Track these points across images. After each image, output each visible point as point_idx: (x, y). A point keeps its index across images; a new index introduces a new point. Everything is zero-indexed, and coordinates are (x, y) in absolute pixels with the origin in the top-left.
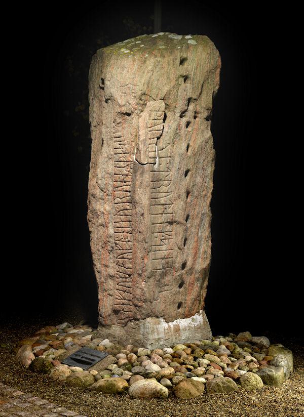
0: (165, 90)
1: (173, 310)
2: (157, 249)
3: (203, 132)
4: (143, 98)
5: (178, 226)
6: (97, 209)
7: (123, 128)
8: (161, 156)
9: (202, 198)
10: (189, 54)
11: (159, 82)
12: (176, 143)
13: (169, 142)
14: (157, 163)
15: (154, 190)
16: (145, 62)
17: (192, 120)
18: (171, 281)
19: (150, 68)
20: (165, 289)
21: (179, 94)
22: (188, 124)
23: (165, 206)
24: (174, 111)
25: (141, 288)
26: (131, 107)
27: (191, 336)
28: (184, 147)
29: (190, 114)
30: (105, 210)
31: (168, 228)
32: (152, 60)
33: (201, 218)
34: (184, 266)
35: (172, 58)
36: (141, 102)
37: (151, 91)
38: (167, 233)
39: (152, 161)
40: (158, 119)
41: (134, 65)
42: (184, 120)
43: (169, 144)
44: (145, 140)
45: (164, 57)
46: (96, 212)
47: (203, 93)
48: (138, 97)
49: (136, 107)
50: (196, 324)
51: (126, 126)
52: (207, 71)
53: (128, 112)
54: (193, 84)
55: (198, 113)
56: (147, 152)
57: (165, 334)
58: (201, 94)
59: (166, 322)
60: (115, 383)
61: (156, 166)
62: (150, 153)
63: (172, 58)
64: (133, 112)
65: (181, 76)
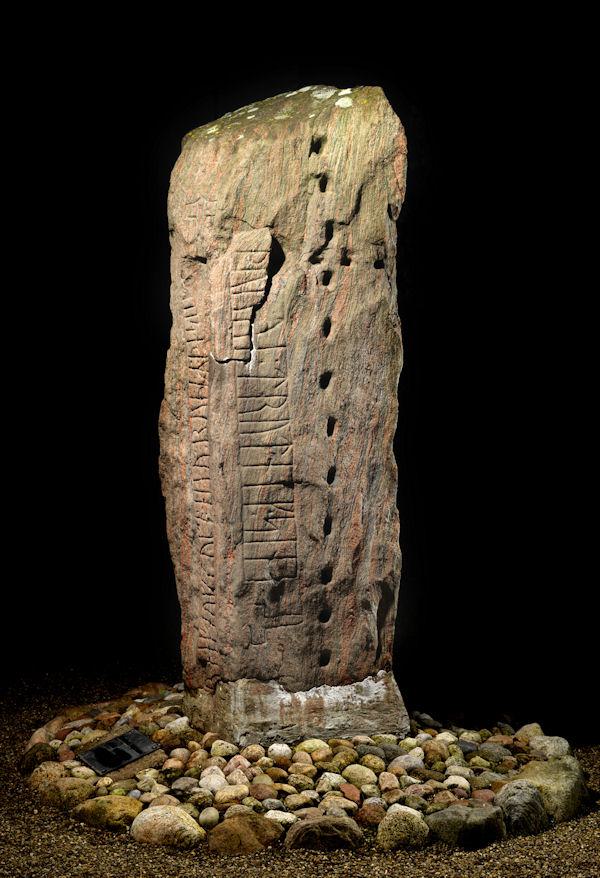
0: (276, 206)
1: (296, 667)
2: (256, 538)
3: (362, 291)
4: (227, 225)
5: (307, 490)
6: (169, 451)
7: (195, 289)
8: (261, 345)
9: (369, 432)
10: (329, 129)
11: (263, 190)
12: (297, 315)
13: (279, 315)
14: (253, 358)
15: (247, 416)
16: (235, 150)
17: (337, 267)
18: (297, 605)
19: (243, 162)
20: (282, 622)
21: (309, 213)
22: (327, 277)
23: (271, 449)
24: (298, 250)
25: (225, 618)
26: (205, 244)
27: (349, 723)
28: (315, 323)
29: (331, 255)
30: (181, 454)
31: (283, 493)
32: (251, 145)
33: (368, 476)
34: (326, 574)
35: (291, 138)
36: (226, 234)
37: (244, 210)
38: (280, 505)
39: (238, 354)
40: (252, 268)
41: (215, 160)
42: (318, 269)
43: (282, 318)
44: (223, 312)
45: (275, 138)
46: (168, 460)
47: (362, 209)
48: (216, 224)
49: (214, 244)
50: (366, 699)
51: (199, 283)
52: (370, 163)
53: (200, 255)
54: (338, 192)
55: (353, 253)
56: (228, 338)
57: (282, 716)
58: (357, 210)
59: (288, 691)
60: (108, 806)
61: (251, 365)
62: (234, 339)
63: (291, 138)
64: (209, 255)
65: (312, 174)
